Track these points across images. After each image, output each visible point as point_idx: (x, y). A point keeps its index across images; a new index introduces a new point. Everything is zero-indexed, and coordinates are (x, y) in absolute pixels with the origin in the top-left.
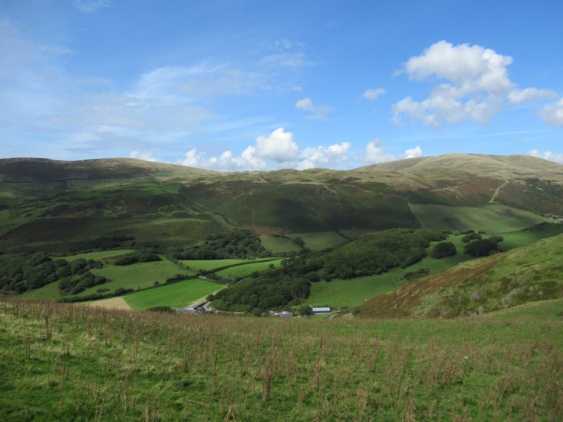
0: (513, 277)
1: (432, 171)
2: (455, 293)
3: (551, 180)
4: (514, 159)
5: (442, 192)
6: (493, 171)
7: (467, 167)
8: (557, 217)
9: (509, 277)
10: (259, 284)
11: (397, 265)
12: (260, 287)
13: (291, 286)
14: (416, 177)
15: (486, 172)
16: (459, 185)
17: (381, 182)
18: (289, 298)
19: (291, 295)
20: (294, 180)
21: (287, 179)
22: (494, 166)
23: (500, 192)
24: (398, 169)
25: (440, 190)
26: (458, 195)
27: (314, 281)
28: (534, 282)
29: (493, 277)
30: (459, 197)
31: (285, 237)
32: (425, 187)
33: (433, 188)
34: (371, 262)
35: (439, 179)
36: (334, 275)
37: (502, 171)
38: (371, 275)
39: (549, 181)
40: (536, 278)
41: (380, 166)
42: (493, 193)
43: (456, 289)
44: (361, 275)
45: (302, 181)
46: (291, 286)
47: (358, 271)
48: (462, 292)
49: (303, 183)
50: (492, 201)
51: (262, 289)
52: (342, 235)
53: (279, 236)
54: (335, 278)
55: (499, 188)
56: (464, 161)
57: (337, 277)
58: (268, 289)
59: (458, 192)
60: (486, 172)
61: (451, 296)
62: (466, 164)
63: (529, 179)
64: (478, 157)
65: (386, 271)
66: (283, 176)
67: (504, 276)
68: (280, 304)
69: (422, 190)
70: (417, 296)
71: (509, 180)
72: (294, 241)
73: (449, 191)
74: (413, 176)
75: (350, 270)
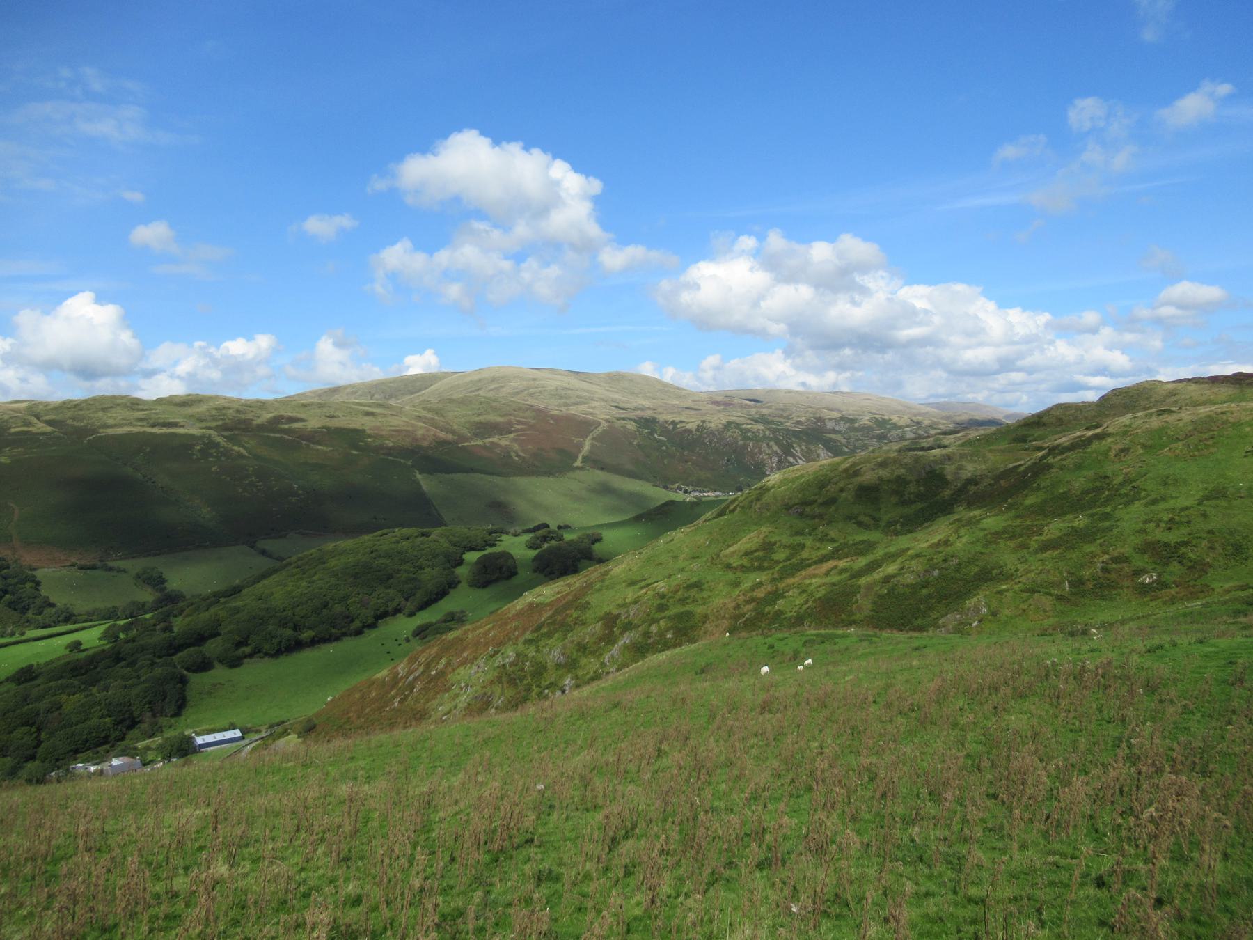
0: (623, 611)
1: (463, 402)
2: (518, 655)
3: (677, 420)
4: (615, 379)
5: (484, 447)
6: (578, 404)
7: (531, 395)
8: (689, 489)
9: (615, 612)
10: (40, 698)
11: (397, 611)
12: (43, 705)
13: (134, 692)
14: (430, 415)
15: (566, 405)
16: (517, 431)
17: (352, 426)
18: (128, 723)
19: (135, 714)
20: (131, 424)
21: (111, 422)
22: (580, 394)
23: (592, 446)
24: (391, 397)
25: (479, 442)
26: (516, 452)
27: (195, 671)
28: (658, 616)
29: (588, 615)
30: (518, 456)
31: (111, 569)
32: (450, 437)
33: (467, 440)
34: (338, 608)
35: (477, 419)
36: (247, 650)
37: (594, 404)
38: (337, 639)
39: (673, 423)
40: (661, 608)
41: (349, 390)
42: (579, 446)
43: (521, 647)
44: (313, 642)
45: (153, 426)
46: (134, 692)
47: (306, 635)
48: (531, 652)
49: (156, 430)
50: (578, 463)
51: (49, 711)
52: (263, 552)
53: (93, 568)
54: (251, 656)
55: (590, 437)
56: (525, 383)
57: (256, 652)
58: (67, 708)
59: (516, 447)
60: (566, 405)
61: (512, 664)
62: (528, 388)
63: (641, 418)
64: (551, 376)
65: (372, 626)
66: (100, 414)
67: (607, 609)
68: (105, 741)
69: (442, 443)
70: (442, 674)
71: (607, 421)
72: (138, 576)
73: (498, 445)
74: (423, 413)
75: (289, 632)
